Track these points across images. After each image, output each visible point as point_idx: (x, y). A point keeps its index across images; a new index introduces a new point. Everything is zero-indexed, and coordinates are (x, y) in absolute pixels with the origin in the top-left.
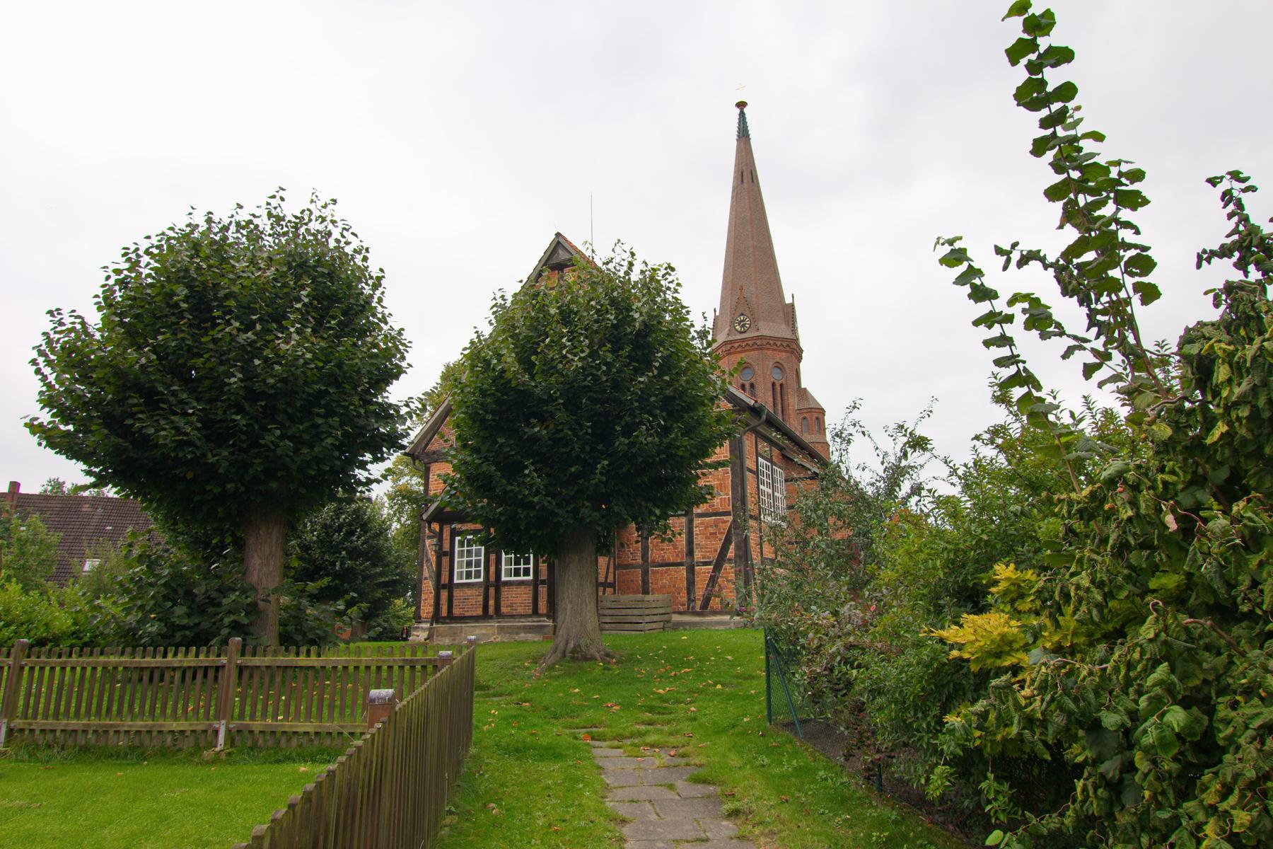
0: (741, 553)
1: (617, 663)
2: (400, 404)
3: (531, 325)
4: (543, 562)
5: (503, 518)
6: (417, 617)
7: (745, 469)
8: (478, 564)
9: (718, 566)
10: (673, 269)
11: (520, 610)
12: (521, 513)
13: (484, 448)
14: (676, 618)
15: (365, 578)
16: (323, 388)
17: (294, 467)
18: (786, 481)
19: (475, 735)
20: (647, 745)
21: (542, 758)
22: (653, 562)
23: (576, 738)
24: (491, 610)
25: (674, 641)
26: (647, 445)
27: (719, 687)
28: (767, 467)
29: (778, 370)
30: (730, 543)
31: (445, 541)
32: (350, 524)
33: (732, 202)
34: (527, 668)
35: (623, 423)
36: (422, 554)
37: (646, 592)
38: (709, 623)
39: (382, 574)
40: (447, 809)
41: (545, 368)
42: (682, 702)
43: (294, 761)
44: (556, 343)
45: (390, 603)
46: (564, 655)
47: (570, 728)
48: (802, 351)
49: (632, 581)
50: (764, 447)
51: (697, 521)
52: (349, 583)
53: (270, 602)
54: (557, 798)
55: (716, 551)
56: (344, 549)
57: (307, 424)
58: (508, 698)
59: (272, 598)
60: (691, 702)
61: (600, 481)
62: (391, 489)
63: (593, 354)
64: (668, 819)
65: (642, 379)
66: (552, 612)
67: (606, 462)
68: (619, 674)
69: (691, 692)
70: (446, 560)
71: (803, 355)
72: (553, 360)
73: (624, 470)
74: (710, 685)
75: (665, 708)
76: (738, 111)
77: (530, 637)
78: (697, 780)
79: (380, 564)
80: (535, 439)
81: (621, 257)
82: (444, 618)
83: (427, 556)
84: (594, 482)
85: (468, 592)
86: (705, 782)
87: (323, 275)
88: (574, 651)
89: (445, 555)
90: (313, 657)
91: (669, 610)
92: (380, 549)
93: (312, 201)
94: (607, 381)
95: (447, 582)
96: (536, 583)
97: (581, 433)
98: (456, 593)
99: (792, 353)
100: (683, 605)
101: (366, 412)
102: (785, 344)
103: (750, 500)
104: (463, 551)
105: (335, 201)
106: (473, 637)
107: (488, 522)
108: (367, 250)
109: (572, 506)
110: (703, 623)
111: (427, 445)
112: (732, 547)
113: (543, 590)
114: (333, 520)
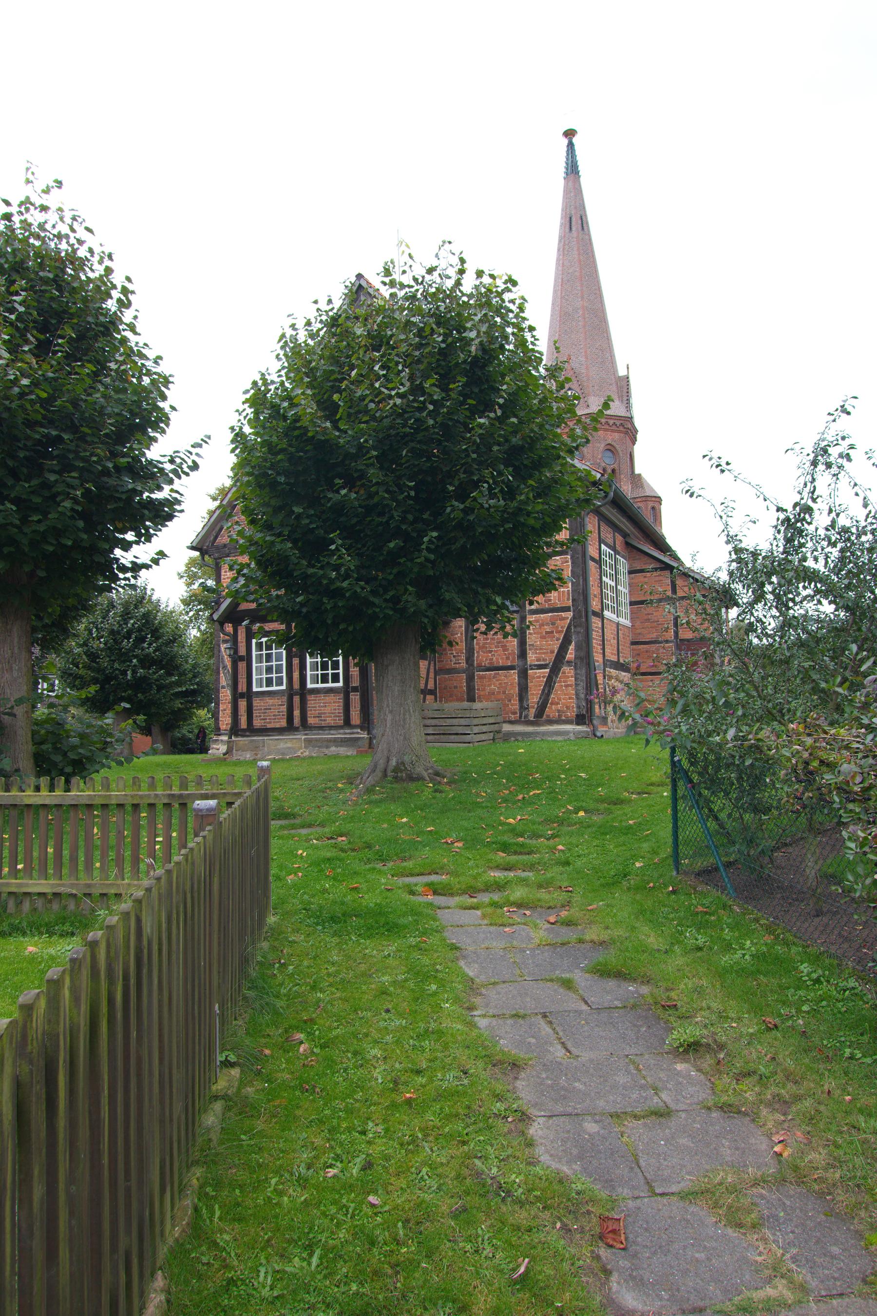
0: (583, 654)
1: (449, 783)
2: (162, 459)
3: (332, 357)
4: (356, 665)
5: (304, 610)
6: (218, 731)
7: (588, 558)
8: (279, 669)
9: (555, 669)
10: (515, 283)
11: (330, 721)
12: (328, 603)
13: (276, 522)
14: (507, 728)
15: (160, 688)
16: (54, 433)
17: (25, 541)
18: (630, 572)
19: (276, 892)
20: (512, 904)
21: (369, 932)
22: (479, 666)
23: (412, 893)
24: (297, 721)
25: (510, 754)
26: (488, 509)
27: (582, 813)
28: (610, 556)
29: (609, 454)
30: (570, 643)
31: (240, 645)
32: (140, 630)
33: (559, 255)
34: (342, 791)
35: (457, 483)
36: (219, 658)
37: (471, 699)
38: (544, 734)
39: (178, 684)
40: (221, 1058)
41: (352, 411)
42: (541, 836)
43: (24, 934)
44: (368, 375)
45: (191, 715)
46: (385, 775)
47: (403, 875)
48: (636, 431)
49: (456, 687)
50: (608, 534)
51: (530, 618)
52: (143, 693)
53: (15, 716)
54: (401, 1016)
55: (552, 652)
56: (135, 657)
57: (35, 482)
58: (319, 830)
59: (19, 711)
60: (553, 837)
61: (427, 560)
62: (185, 594)
63: (417, 390)
64: (586, 1056)
65: (482, 421)
66: (367, 723)
67: (435, 534)
68: (453, 798)
69: (548, 821)
70: (242, 665)
71: (639, 436)
72: (363, 398)
73: (458, 545)
74: (570, 812)
75: (522, 845)
76: (565, 141)
77: (342, 750)
78: (603, 972)
79: (176, 672)
80: (340, 509)
81: (448, 264)
82: (243, 730)
83: (223, 662)
84: (419, 560)
85: (270, 701)
86: (619, 975)
87: (45, 281)
88: (396, 770)
89: (240, 660)
90: (44, 792)
91: (500, 719)
92: (173, 658)
93: (28, 182)
94: (433, 427)
95: (245, 690)
96: (347, 690)
97: (401, 497)
98: (256, 702)
99: (626, 433)
100: (515, 713)
101: (116, 467)
102: (618, 423)
103: (594, 590)
104: (261, 655)
105: (59, 184)
106: (265, 763)
107: (285, 616)
108: (110, 257)
109: (391, 593)
110: (537, 733)
111: (216, 537)
112: (572, 647)
113: (355, 698)
114: (120, 625)
